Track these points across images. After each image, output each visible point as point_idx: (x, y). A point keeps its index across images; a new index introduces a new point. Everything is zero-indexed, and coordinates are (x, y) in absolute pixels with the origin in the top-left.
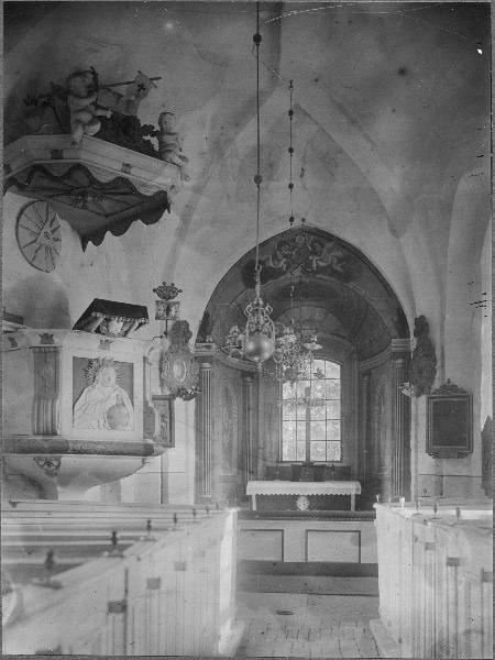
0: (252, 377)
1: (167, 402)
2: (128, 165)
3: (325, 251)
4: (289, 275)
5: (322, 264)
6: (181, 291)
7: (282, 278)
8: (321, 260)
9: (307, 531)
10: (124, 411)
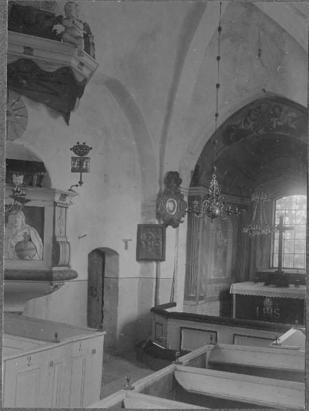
0: (247, 210)
1: (160, 230)
2: (28, 48)
3: (282, 113)
4: (255, 134)
5: (280, 124)
6: (91, 148)
7: (251, 136)
8: (279, 121)
9: (235, 335)
10: (30, 245)
